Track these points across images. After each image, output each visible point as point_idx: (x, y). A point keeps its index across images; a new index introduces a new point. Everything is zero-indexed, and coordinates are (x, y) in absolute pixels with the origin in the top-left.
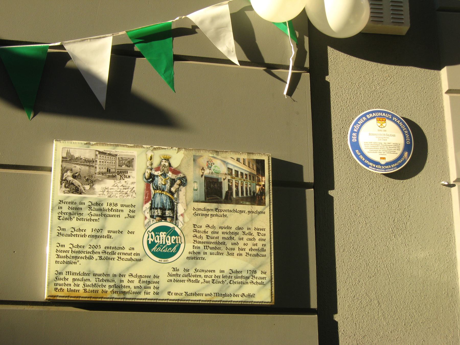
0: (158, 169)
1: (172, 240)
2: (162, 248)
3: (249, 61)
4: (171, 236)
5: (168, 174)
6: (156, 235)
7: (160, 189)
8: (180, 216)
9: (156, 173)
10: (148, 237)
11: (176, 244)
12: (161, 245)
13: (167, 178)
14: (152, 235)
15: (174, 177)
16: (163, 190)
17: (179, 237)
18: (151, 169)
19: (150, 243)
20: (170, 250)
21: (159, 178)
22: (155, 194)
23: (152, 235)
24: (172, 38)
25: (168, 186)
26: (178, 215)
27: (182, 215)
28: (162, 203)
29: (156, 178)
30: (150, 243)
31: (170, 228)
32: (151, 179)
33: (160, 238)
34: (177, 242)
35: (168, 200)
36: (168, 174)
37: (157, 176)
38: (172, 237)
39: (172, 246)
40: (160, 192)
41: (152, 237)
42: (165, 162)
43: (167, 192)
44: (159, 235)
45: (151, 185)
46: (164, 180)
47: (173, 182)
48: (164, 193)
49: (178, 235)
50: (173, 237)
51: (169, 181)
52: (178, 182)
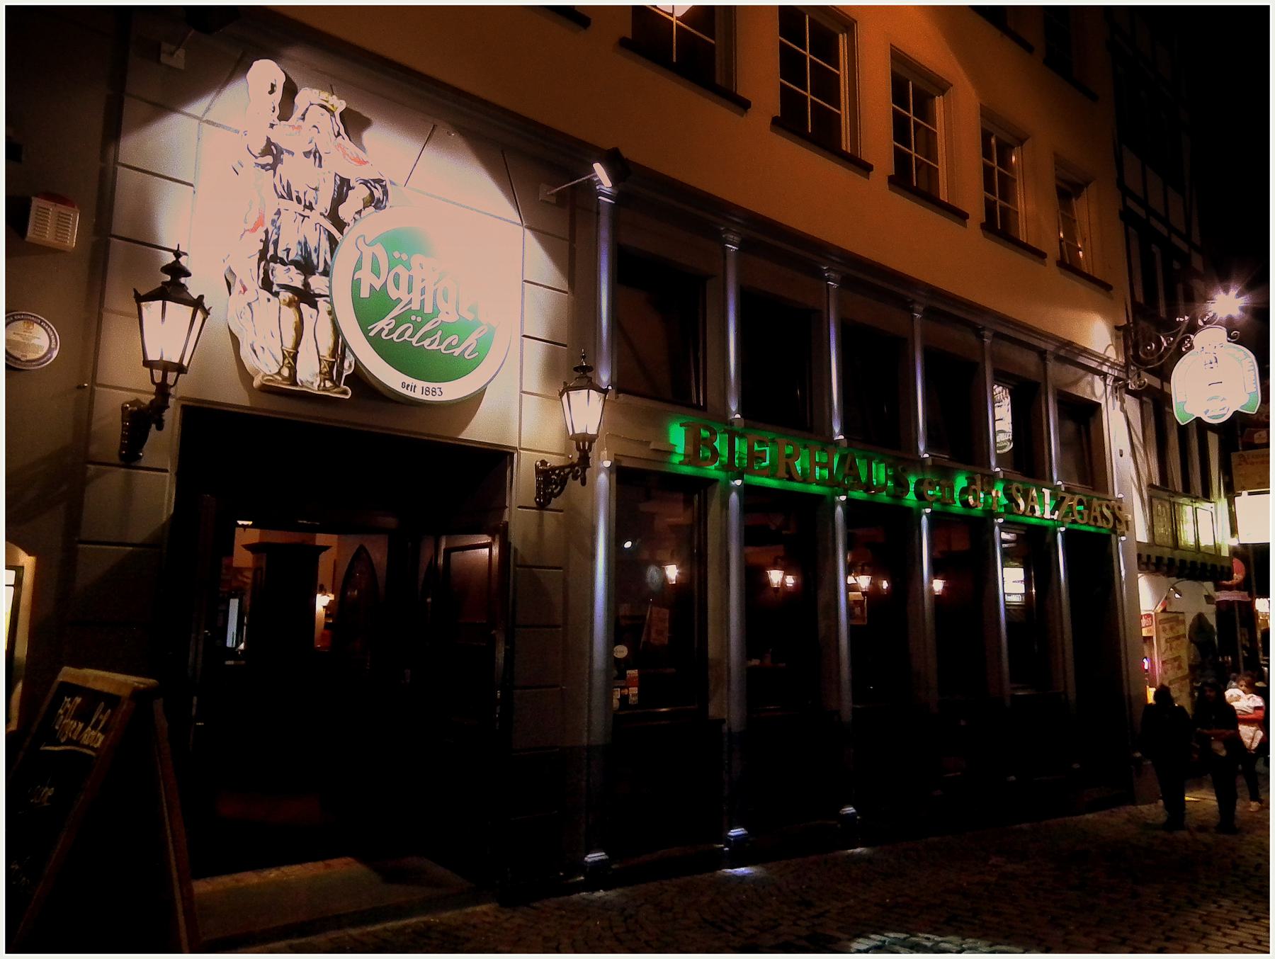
10: (358, 267)
12: (416, 313)
14: (374, 257)
16: (310, 207)
19: (365, 293)
20: (449, 346)
23: (374, 257)
24: (120, 168)
30: (365, 293)
35: (324, 237)
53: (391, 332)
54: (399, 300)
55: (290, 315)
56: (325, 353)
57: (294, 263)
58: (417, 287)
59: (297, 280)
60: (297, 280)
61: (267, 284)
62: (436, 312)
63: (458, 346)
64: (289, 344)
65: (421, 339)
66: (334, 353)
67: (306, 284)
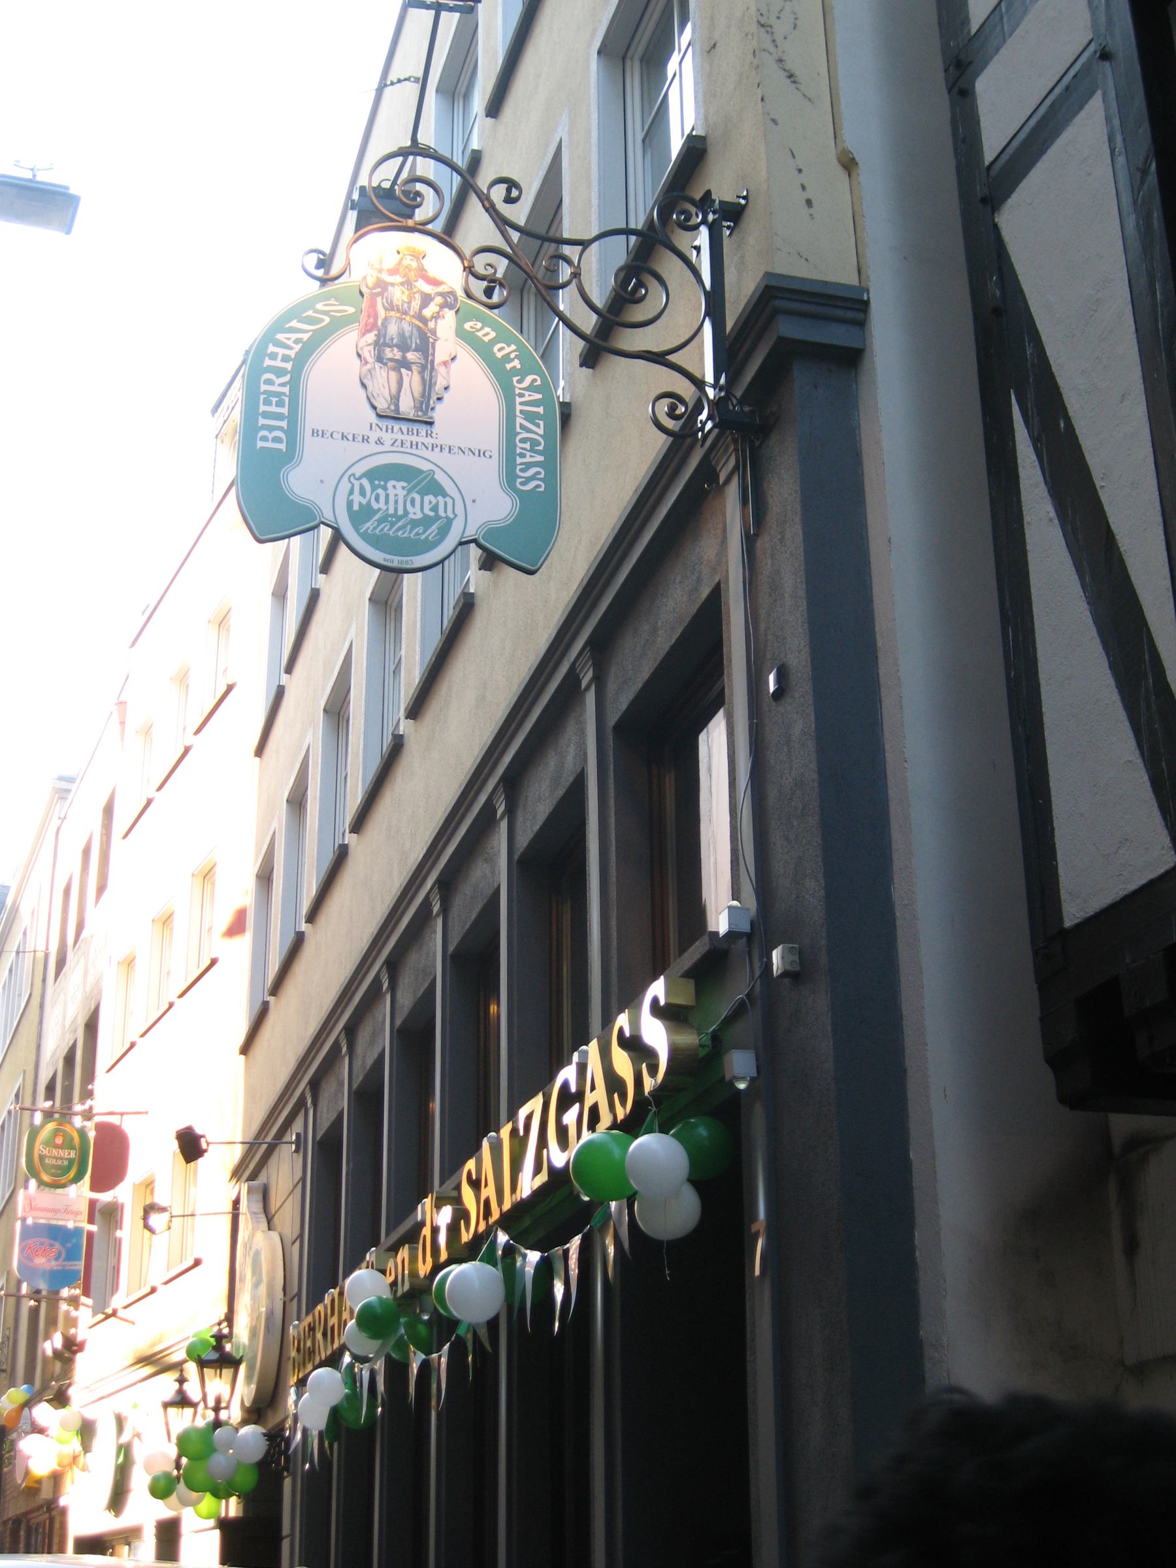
0: (393, 272)
2: (392, 524)
3: (989, 156)
4: (423, 494)
5: (417, 284)
6: (374, 488)
7: (398, 311)
8: (439, 364)
9: (390, 279)
10: (351, 492)
12: (391, 516)
14: (362, 487)
15: (428, 289)
17: (448, 499)
18: (380, 271)
19: (356, 507)
22: (386, 319)
23: (362, 487)
25: (416, 304)
26: (436, 362)
27: (445, 363)
28: (401, 335)
29: (390, 288)
30: (356, 507)
31: (421, 472)
33: (387, 496)
34: (441, 513)
36: (417, 284)
37: (393, 285)
38: (427, 498)
39: (426, 522)
41: (363, 492)
44: (385, 488)
45: (379, 300)
47: (427, 300)
48: (408, 318)
49: (445, 495)
50: (431, 497)
51: (417, 296)
52: (439, 300)
53: (375, 528)
54: (380, 509)
55: (393, 376)
56: (417, 395)
57: (396, 346)
58: (392, 499)
59: (397, 354)
60: (397, 354)
61: (380, 359)
62: (406, 513)
63: (424, 533)
64: (394, 391)
65: (398, 530)
66: (423, 396)
67: (404, 357)
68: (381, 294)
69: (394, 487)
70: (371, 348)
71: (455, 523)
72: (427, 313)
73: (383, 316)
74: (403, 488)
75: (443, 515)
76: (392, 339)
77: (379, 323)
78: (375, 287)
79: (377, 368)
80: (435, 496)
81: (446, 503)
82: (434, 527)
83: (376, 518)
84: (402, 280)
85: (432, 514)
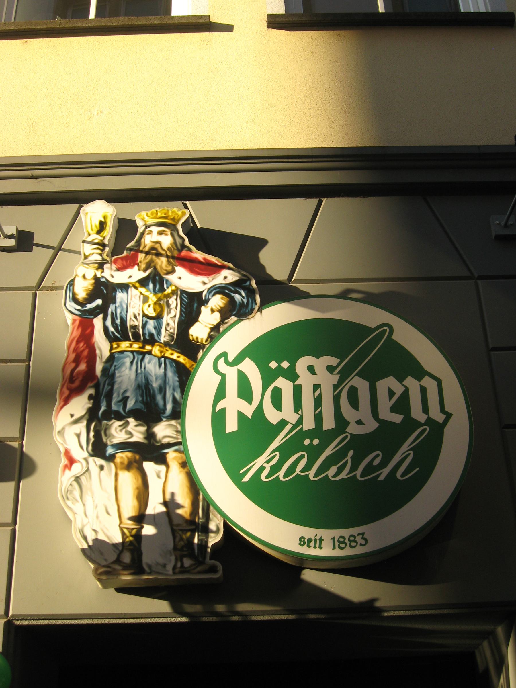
1: (384, 405)
4: (372, 376)
6: (268, 377)
7: (136, 337)
9: (119, 277)
11: (410, 424)
13: (168, 291)
17: (427, 381)
19: (232, 425)
20: (370, 469)
21: (132, 291)
22: (111, 358)
25: (171, 320)
28: (144, 388)
29: (120, 296)
30: (232, 425)
32: (99, 302)
33: (297, 391)
34: (417, 413)
37: (125, 287)
38: (384, 385)
39: (386, 438)
40: (136, 346)
41: (245, 392)
42: (160, 233)
43: (166, 344)
44: (291, 375)
45: (98, 322)
46: (153, 298)
48: (156, 350)
49: (420, 373)
50: (388, 383)
52: (217, 301)
53: (275, 469)
54: (283, 423)
55: (128, 480)
59: (137, 433)
60: (137, 433)
61: (98, 449)
63: (383, 464)
67: (150, 435)
68: (102, 310)
69: (311, 369)
70: (82, 427)
71: (447, 431)
72: (199, 332)
73: (106, 354)
74: (330, 369)
75: (422, 418)
76: (124, 400)
77: (99, 368)
78: (91, 297)
79: (94, 469)
80: (401, 379)
81: (423, 390)
82: (405, 447)
83: (276, 443)
84: (143, 275)
85: (397, 418)
